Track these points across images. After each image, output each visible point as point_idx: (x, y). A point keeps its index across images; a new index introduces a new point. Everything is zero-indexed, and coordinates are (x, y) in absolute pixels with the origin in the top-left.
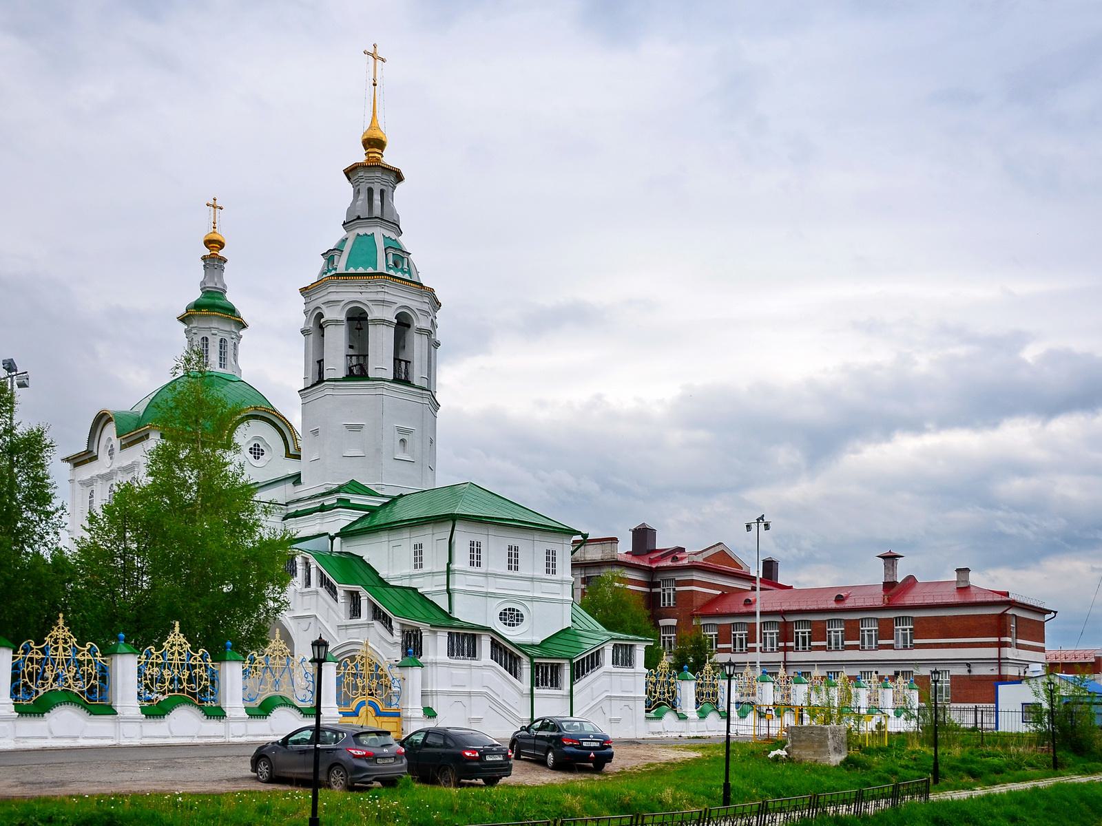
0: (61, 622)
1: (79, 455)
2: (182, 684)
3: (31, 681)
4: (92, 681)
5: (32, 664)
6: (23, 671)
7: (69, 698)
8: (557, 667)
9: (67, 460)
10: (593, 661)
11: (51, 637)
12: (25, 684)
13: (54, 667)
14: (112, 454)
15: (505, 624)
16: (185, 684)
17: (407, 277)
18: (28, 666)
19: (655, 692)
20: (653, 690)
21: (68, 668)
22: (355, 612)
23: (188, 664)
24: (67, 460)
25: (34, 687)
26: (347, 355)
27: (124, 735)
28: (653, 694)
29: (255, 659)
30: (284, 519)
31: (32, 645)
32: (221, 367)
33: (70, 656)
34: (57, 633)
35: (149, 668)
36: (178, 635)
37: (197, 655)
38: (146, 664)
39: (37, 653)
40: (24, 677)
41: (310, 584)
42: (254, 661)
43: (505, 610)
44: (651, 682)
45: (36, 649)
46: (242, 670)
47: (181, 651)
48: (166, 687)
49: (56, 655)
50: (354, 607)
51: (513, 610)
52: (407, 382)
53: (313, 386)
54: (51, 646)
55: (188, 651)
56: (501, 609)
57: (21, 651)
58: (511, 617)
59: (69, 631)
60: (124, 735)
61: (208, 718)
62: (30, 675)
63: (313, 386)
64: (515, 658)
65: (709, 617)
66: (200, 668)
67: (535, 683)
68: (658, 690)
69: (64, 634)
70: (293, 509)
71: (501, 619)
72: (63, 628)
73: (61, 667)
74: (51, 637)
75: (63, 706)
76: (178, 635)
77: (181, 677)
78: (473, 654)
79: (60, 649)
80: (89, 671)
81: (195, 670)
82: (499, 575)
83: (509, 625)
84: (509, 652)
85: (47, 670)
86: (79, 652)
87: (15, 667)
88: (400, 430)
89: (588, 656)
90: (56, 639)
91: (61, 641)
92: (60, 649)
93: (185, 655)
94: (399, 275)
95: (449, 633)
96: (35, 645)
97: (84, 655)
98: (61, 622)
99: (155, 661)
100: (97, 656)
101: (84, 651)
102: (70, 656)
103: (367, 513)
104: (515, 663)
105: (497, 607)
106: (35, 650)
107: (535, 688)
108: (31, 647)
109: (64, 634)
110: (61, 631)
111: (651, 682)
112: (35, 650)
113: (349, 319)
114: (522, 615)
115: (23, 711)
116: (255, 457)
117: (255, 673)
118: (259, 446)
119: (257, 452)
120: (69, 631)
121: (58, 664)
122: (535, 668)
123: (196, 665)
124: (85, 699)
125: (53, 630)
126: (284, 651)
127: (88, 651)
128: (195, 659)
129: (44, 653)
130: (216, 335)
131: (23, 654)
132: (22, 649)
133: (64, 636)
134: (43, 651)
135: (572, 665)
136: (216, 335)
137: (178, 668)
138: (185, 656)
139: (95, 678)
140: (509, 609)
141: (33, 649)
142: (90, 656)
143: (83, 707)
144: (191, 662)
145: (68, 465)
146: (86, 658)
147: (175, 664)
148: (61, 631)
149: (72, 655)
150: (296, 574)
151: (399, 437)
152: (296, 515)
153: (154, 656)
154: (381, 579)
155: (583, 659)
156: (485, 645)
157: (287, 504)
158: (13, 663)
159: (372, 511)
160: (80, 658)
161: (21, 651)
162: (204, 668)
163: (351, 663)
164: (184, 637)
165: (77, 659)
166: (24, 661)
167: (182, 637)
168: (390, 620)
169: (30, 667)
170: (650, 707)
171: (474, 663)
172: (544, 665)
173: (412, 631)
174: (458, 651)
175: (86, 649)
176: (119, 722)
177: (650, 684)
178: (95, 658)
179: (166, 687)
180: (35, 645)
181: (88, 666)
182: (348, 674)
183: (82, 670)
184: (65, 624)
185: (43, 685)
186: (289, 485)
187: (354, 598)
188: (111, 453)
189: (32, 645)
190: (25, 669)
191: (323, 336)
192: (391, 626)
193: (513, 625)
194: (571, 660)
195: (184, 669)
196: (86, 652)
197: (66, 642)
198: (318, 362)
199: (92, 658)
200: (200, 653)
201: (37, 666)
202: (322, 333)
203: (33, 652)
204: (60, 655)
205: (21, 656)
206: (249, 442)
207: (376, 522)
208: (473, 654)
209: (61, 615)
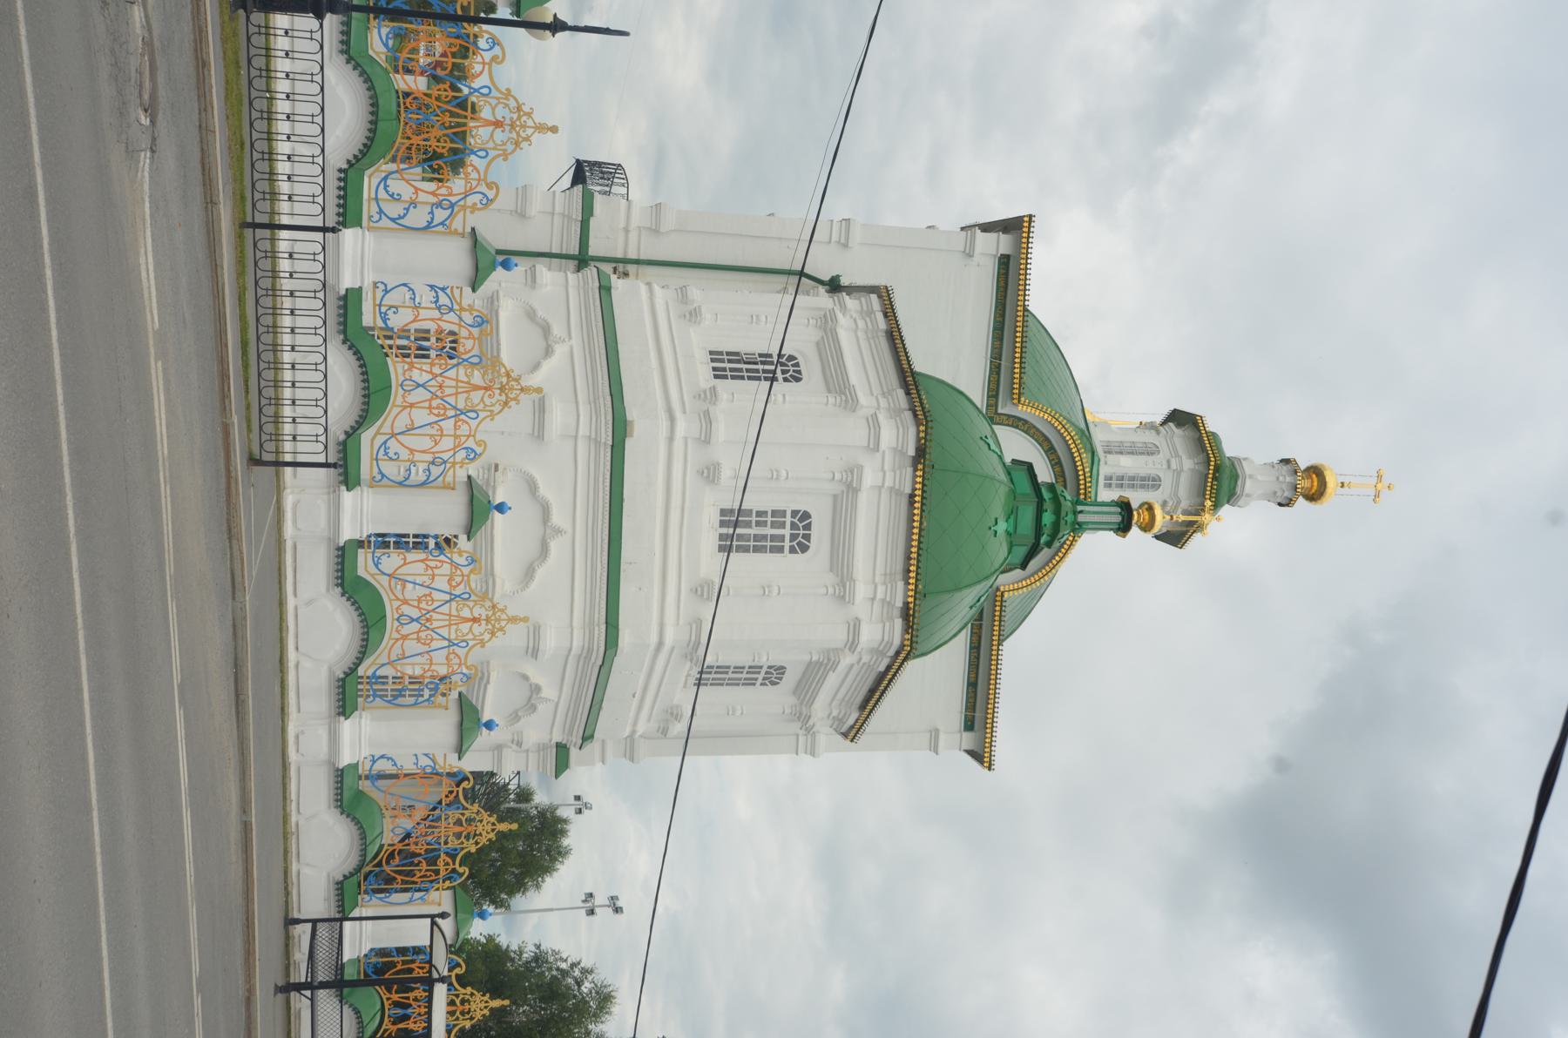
4: (399, 878)
31: (458, 971)
34: (478, 1001)
35: (422, 968)
36: (486, 1007)
40: (404, 962)
45: (458, 791)
55: (463, 849)
61: (340, 170)
69: (484, 833)
72: (493, 830)
74: (472, 994)
75: (360, 643)
76: (486, 1007)
77: (412, 1020)
79: (458, 829)
81: (424, 863)
85: (442, 86)
86: (453, 857)
90: (468, 1001)
92: (458, 829)
96: (464, 789)
98: (496, 1003)
101: (454, 864)
106: (455, 789)
125: (483, 995)
127: (454, 871)
130: (1169, 467)
136: (1169, 467)
142: (445, 873)
144: (443, 856)
146: (442, 868)
160: (441, 860)
162: (434, 878)
163: (457, 975)
164: (484, 1015)
165: (439, 856)
167: (482, 1013)
175: (457, 866)
176: (329, 493)
180: (464, 789)
184: (492, 1010)
196: (452, 866)
199: (441, 876)
200: (461, 870)
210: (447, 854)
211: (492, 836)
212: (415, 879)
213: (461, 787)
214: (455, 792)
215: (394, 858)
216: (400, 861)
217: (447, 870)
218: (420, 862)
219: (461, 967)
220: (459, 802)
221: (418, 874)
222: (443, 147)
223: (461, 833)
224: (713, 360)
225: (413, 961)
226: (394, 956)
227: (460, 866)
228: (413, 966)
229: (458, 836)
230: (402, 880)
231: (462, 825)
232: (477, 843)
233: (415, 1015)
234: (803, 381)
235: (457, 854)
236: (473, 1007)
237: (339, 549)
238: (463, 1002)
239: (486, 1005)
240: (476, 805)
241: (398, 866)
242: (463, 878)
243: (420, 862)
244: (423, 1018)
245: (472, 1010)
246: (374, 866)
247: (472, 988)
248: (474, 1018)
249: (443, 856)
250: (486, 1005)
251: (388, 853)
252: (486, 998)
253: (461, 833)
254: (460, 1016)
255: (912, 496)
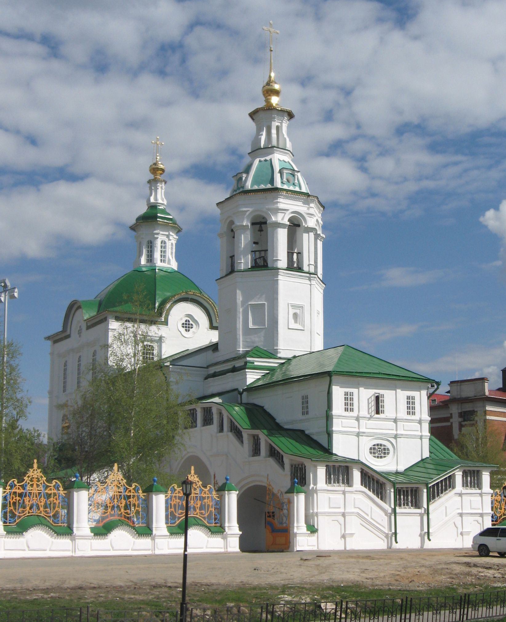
0: (35, 466)
1: (57, 334)
2: (120, 510)
3: (15, 509)
4: (56, 509)
5: (16, 497)
6: (10, 502)
7: (40, 522)
8: (416, 491)
9: (48, 338)
10: (449, 483)
11: (29, 477)
12: (11, 511)
13: (30, 499)
14: (80, 333)
15: (375, 457)
16: (198, 511)
17: (297, 189)
18: (13, 498)
19: (501, 509)
20: (499, 507)
21: (40, 500)
22: (256, 451)
23: (124, 495)
24: (48, 338)
25: (17, 514)
26: (252, 251)
27: (78, 549)
28: (499, 510)
29: (175, 490)
30: (206, 378)
31: (16, 482)
32: (161, 262)
33: (41, 490)
37: (131, 488)
38: (171, 497)
39: (19, 488)
40: (171, 508)
41: (223, 429)
42: (175, 491)
43: (374, 445)
44: (496, 501)
45: (19, 486)
46: (88, 497)
47: (195, 487)
48: (109, 513)
49: (32, 490)
50: (255, 446)
51: (381, 445)
52: (299, 269)
53: (227, 275)
54: (29, 483)
55: (124, 485)
56: (371, 445)
57: (8, 487)
58: (379, 451)
59: (41, 472)
60: (78, 549)
61: (139, 536)
62: (14, 504)
63: (227, 275)
64: (381, 484)
65: (331, 442)
66: (208, 499)
67: (398, 503)
68: (503, 507)
69: (38, 474)
70: (212, 370)
71: (371, 453)
72: (194, 476)
73: (35, 498)
74: (29, 477)
76: (194, 476)
78: (348, 482)
79: (35, 486)
80: (54, 502)
81: (130, 500)
82: (343, 416)
83: (378, 457)
84: (375, 479)
87: (5, 498)
88: (294, 306)
89: (442, 481)
91: (35, 479)
92: (35, 486)
93: (198, 490)
94: (292, 188)
95: (327, 466)
97: (51, 489)
98: (35, 466)
99: (177, 495)
100: (60, 490)
101: (51, 486)
102: (41, 490)
103: (268, 372)
104: (382, 488)
105: (367, 443)
106: (17, 487)
107: (397, 508)
108: (14, 484)
109: (38, 474)
110: (35, 472)
111: (496, 501)
112: (17, 487)
113: (253, 224)
114: (388, 449)
115: (10, 532)
116: (186, 330)
117: (175, 501)
118: (189, 321)
119: (187, 326)
120: (41, 472)
121: (33, 497)
122: (398, 492)
123: (130, 495)
124: (51, 522)
126: (197, 483)
127: (54, 486)
128: (205, 493)
129: (24, 489)
131: (9, 489)
132: (170, 490)
133: (38, 476)
134: (23, 487)
135: (428, 489)
137: (193, 500)
138: (122, 489)
139: (59, 507)
140: (378, 445)
141: (16, 485)
143: (50, 528)
145: (49, 343)
146: (52, 492)
147: (34, 493)
148: (35, 472)
149: (42, 489)
150: (213, 422)
151: (292, 311)
152: (215, 375)
153: (177, 492)
154: (278, 425)
155: (438, 484)
156: (357, 475)
157: (208, 367)
158: (2, 496)
159: (272, 370)
161: (8, 487)
163: (18, 483)
166: (10, 494)
168: (282, 456)
169: (14, 499)
170: (496, 521)
171: (348, 489)
172: (405, 489)
173: (299, 465)
174: (471, 484)
177: (495, 502)
178: (59, 492)
179: (109, 513)
181: (54, 498)
182: (175, 497)
183: (49, 501)
184: (38, 468)
185: (23, 512)
186: (210, 352)
187: (256, 442)
188: (80, 332)
189: (16, 482)
190: (11, 500)
191: (234, 237)
192: (283, 461)
193: (381, 457)
194: (427, 485)
195: (121, 499)
196: (52, 488)
197: (38, 481)
198: (230, 257)
200: (134, 487)
201: (19, 498)
202: (233, 236)
203: (16, 488)
204: (35, 490)
205: (8, 491)
206: (181, 319)
207: (275, 379)
208: (348, 482)
209: (35, 461)
210: (126, 492)
211: (196, 476)
212: (57, 503)
213: (176, 489)
214: (19, 487)
215: (202, 513)
216: (128, 509)
217: (53, 489)
218: (129, 501)
219: (175, 486)
220: (23, 485)
221: (135, 502)
222: (43, 500)
223: (37, 484)
224: (348, 411)
225: (171, 504)
226: (7, 511)
227: (52, 484)
228: (173, 504)
229: (38, 485)
230: (9, 507)
231: (33, 484)
232: (42, 477)
233: (37, 502)
234: (193, 328)
235: (46, 485)
236: (35, 476)
237: (95, 535)
238: (31, 481)
239: (35, 470)
240: (25, 478)
241: (51, 509)
242: (137, 485)
243: (49, 501)
244: (195, 501)
245: (37, 477)
246: (205, 520)
247: (25, 476)
248: (41, 476)
249: (46, 491)
250: (35, 470)
251: (200, 515)
252: (31, 470)
253: (37, 484)
254: (40, 482)
255: (273, 267)
